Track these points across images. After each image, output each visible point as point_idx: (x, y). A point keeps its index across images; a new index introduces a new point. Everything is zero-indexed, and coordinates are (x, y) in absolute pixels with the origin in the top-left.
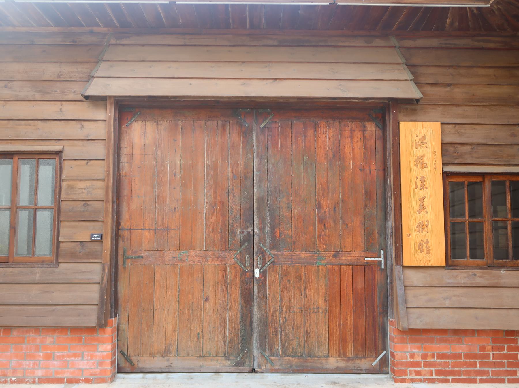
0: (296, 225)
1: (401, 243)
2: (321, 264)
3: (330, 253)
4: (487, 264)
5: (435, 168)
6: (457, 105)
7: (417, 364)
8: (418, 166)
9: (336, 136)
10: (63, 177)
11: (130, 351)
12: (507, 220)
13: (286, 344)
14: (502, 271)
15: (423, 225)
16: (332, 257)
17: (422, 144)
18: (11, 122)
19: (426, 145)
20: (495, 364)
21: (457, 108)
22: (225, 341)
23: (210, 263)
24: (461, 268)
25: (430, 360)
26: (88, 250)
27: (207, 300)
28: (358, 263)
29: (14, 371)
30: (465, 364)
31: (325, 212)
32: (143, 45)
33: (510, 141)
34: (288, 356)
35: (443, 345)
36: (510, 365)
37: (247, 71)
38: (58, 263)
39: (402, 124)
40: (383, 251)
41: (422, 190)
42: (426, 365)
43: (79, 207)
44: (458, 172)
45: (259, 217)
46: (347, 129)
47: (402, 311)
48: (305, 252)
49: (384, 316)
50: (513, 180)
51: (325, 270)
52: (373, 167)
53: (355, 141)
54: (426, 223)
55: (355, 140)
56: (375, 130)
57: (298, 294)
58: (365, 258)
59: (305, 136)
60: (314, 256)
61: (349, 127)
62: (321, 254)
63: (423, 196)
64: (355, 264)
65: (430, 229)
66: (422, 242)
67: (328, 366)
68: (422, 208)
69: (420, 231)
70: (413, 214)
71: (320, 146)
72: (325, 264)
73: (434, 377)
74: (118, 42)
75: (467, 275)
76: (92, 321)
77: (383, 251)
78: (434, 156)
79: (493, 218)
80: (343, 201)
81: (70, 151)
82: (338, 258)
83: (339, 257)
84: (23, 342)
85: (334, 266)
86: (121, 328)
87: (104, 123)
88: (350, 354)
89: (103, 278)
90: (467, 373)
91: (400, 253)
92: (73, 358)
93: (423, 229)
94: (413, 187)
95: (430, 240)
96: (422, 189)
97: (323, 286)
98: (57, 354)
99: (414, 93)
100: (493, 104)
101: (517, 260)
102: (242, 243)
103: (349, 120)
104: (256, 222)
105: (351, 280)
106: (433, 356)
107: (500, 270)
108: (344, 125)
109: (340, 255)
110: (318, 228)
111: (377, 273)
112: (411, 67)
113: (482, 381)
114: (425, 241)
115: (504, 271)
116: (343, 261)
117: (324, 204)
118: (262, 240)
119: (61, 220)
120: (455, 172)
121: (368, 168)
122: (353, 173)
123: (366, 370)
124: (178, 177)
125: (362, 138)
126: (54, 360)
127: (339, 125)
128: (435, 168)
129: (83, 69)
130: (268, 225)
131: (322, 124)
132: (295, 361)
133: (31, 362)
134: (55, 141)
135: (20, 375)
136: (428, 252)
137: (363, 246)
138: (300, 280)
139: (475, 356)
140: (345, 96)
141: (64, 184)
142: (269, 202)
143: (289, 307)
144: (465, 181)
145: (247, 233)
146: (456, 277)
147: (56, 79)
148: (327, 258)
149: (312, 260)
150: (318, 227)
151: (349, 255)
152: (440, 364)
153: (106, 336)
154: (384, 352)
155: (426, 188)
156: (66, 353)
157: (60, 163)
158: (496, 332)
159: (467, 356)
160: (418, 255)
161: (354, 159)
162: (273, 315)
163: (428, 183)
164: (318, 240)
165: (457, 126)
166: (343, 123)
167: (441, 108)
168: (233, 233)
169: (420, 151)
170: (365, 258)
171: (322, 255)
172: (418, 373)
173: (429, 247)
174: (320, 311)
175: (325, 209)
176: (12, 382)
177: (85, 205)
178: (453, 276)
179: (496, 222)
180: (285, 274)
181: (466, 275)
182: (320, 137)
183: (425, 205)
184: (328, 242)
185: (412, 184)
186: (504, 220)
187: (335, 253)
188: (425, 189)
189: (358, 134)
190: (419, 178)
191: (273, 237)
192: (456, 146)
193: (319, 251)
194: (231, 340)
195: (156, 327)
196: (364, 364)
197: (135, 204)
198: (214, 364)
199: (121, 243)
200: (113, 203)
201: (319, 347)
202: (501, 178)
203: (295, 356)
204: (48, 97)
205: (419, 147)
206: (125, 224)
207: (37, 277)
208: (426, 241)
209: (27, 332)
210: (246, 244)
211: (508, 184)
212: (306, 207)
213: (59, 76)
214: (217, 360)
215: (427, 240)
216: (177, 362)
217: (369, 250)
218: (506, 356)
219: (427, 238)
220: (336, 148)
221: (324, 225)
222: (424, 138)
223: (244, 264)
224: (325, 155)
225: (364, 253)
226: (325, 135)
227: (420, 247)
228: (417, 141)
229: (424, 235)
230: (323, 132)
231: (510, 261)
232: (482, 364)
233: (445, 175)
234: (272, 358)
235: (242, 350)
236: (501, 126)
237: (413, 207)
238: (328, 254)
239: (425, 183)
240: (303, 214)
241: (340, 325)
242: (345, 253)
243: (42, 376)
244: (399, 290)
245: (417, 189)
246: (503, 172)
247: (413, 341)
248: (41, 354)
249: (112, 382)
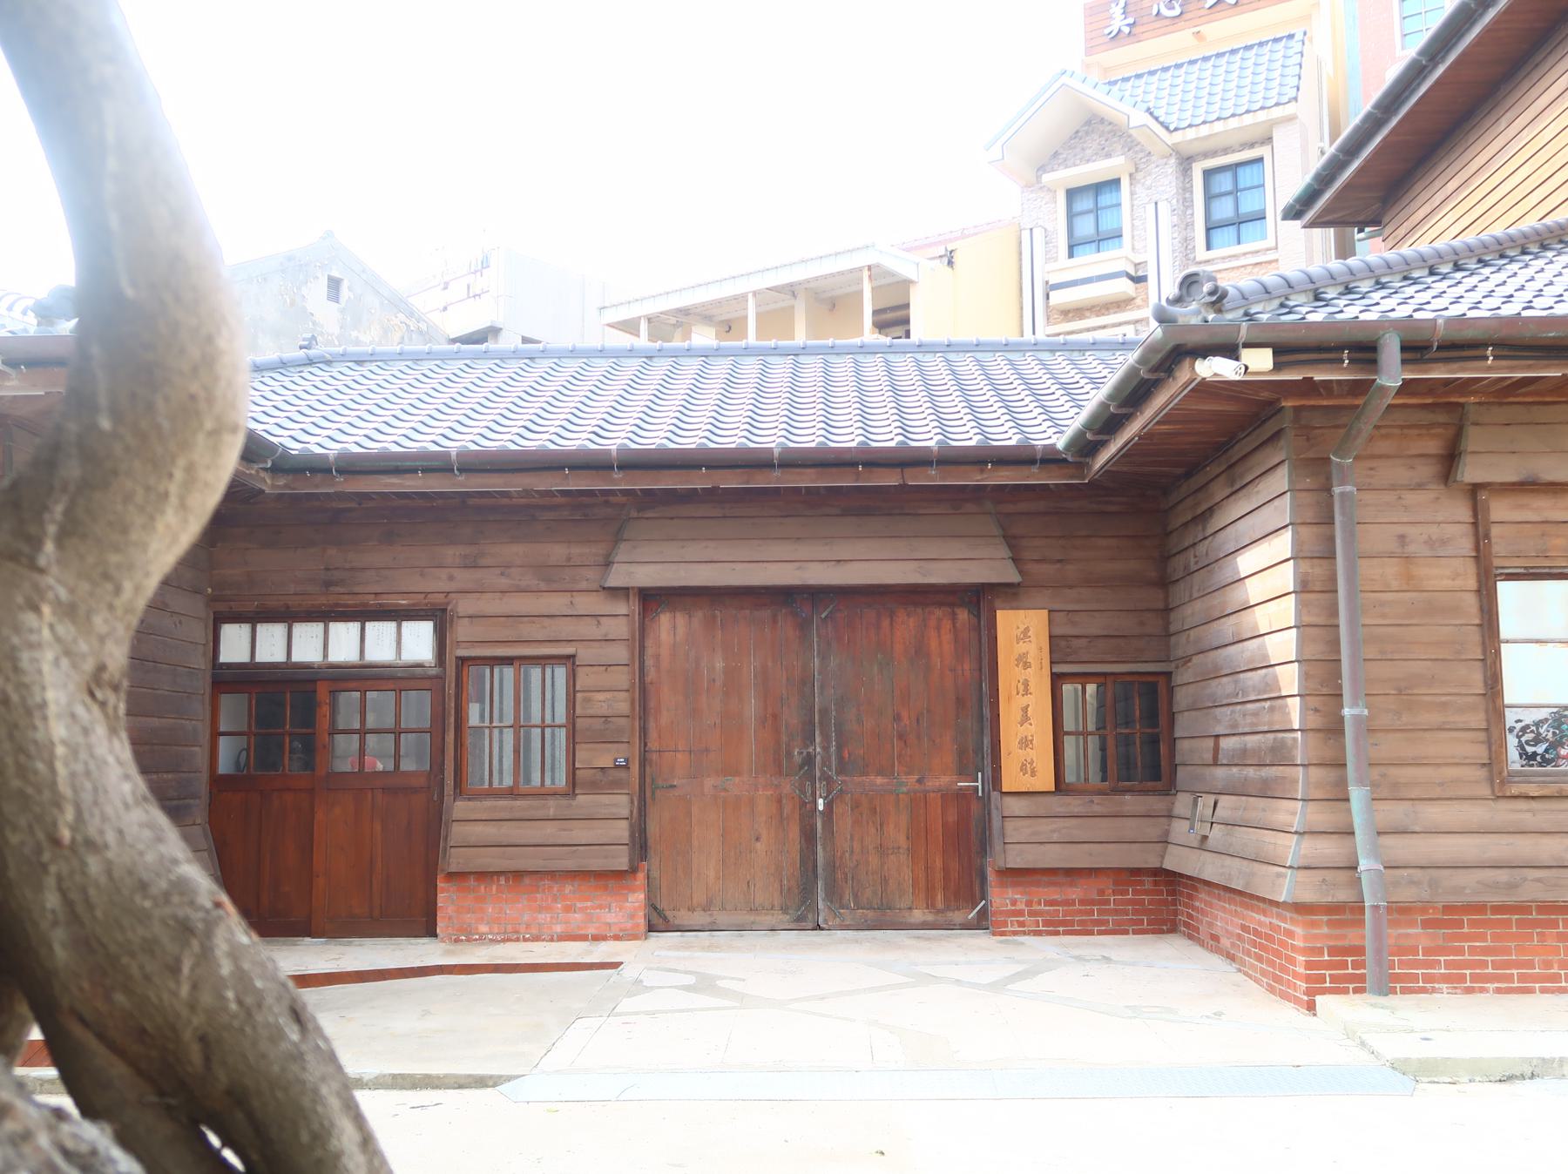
5: (1042, 668)
6: (1070, 587)
7: (1020, 913)
10: (577, 689)
11: (663, 904)
13: (859, 894)
18: (510, 618)
20: (1116, 912)
22: (781, 893)
23: (760, 793)
25: (1035, 907)
26: (611, 778)
27: (758, 839)
29: (528, 926)
30: (1081, 912)
32: (672, 518)
34: (862, 909)
35: (1052, 889)
36: (1136, 912)
37: (804, 551)
38: (575, 795)
39: (999, 613)
40: (980, 774)
42: (1032, 913)
43: (598, 724)
45: (822, 733)
47: (998, 847)
49: (983, 857)
52: (967, 666)
54: (1030, 738)
57: (873, 830)
67: (912, 920)
68: (1025, 719)
73: (1041, 928)
74: (640, 515)
76: (622, 863)
77: (980, 774)
81: (585, 654)
84: (537, 892)
85: (918, 795)
86: (651, 876)
87: (625, 618)
88: (940, 905)
89: (632, 812)
90: (1081, 923)
92: (598, 911)
93: (1027, 746)
95: (1034, 759)
97: (904, 819)
98: (579, 905)
99: (1012, 576)
102: (801, 767)
104: (818, 740)
105: (939, 811)
106: (1040, 904)
112: (1012, 541)
113: (1101, 933)
114: (1029, 760)
117: (904, 714)
118: (826, 762)
119: (576, 741)
123: (960, 924)
124: (719, 683)
126: (575, 912)
129: (598, 550)
130: (834, 743)
132: (870, 914)
133: (548, 915)
134: (565, 643)
135: (535, 931)
136: (1033, 774)
138: (876, 812)
139: (1092, 902)
140: (926, 582)
141: (579, 695)
142: (834, 713)
143: (862, 847)
145: (37, 315)
147: (564, 564)
152: (1048, 912)
153: (638, 883)
154: (984, 902)
155: (1030, 693)
156: (589, 904)
157: (573, 670)
158: (1118, 871)
159: (1082, 902)
162: (841, 858)
163: (1032, 689)
168: (789, 754)
169: (1022, 647)
172: (1021, 924)
174: (901, 851)
175: (906, 721)
176: (525, 940)
177: (606, 722)
180: (856, 805)
189: (947, 624)
190: (1021, 681)
191: (840, 759)
192: (1069, 639)
194: (789, 889)
195: (695, 875)
196: (958, 917)
197: (665, 719)
198: (769, 919)
199: (648, 769)
200: (640, 718)
201: (900, 897)
202: (1128, 678)
203: (871, 908)
204: (555, 586)
206: (653, 744)
207: (551, 813)
209: (542, 879)
210: (806, 768)
213: (569, 559)
214: (773, 915)
216: (722, 918)
217: (963, 772)
218: (1131, 902)
222: (1027, 630)
223: (804, 793)
227: (1023, 768)
232: (1100, 912)
234: (842, 911)
235: (803, 903)
241: (927, 868)
243: (562, 932)
244: (996, 822)
247: (1014, 885)
248: (559, 906)
249: (646, 939)
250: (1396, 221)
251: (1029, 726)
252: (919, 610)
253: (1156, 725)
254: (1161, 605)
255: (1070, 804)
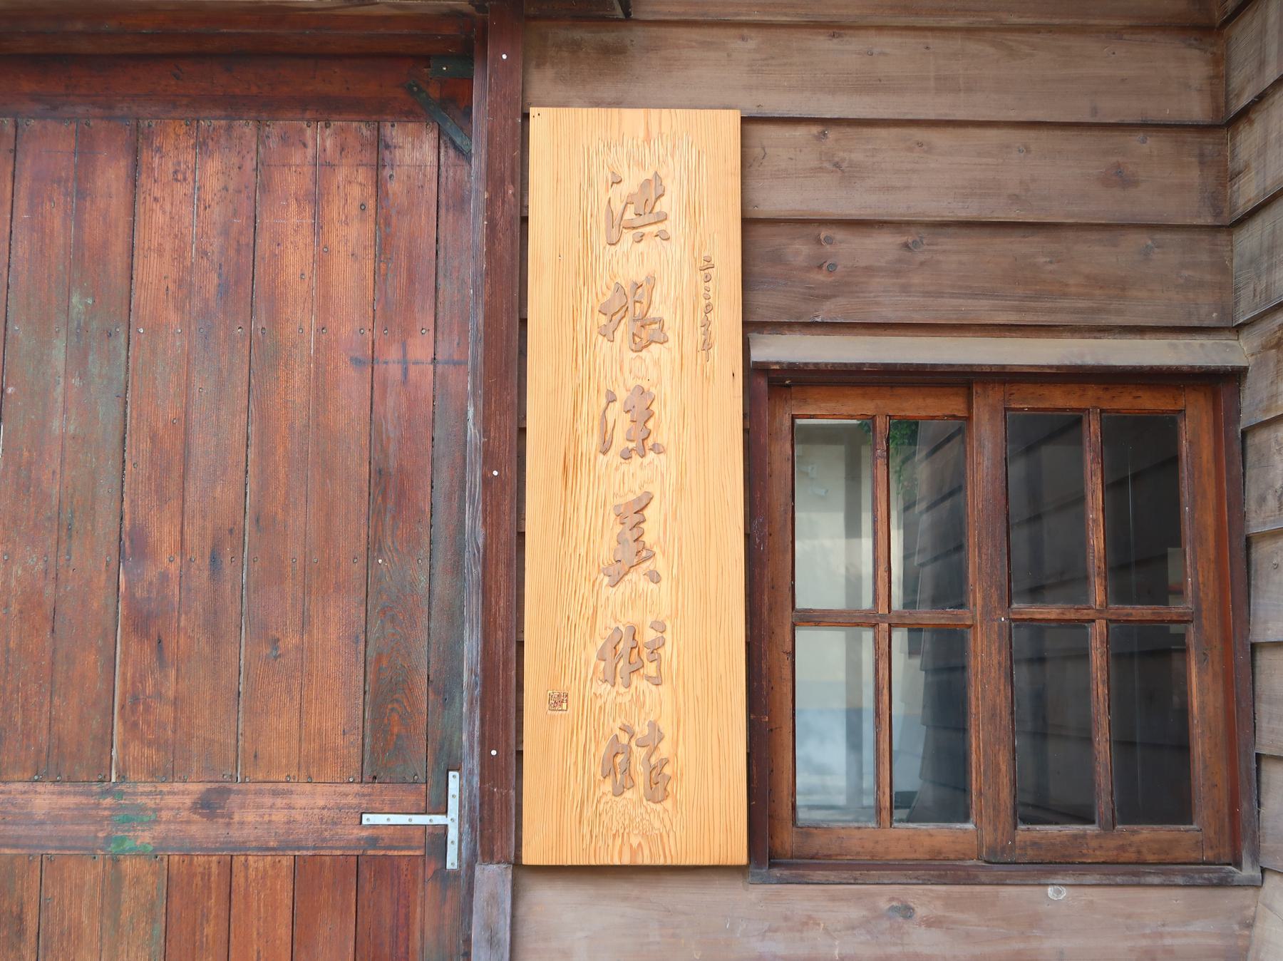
0: (12, 645)
1: (513, 742)
2: (131, 849)
3: (183, 793)
4: (980, 846)
5: (707, 346)
6: (835, 28)
8: (618, 334)
9: (240, 192)
12: (1086, 614)
14: (1050, 890)
15: (631, 644)
16: (190, 809)
17: (639, 221)
19: (661, 226)
21: (835, 40)
24: (832, 875)
28: (324, 840)
31: (164, 577)
33: (1105, 205)
41: (636, 459)
44: (826, 364)
46: (296, 157)
48: (50, 787)
50: (1118, 411)
51: (150, 879)
53: (335, 216)
54: (649, 635)
55: (334, 211)
56: (436, 163)
58: (365, 816)
59: (82, 194)
60: (97, 806)
61: (305, 145)
62: (134, 794)
63: (639, 493)
64: (307, 849)
65: (670, 666)
66: (624, 739)
69: (619, 680)
70: (585, 589)
71: (155, 244)
72: (150, 848)
75: (865, 913)
78: (702, 285)
79: (1015, 605)
80: (258, 521)
82: (223, 816)
83: (225, 811)
91: (507, 795)
94: (590, 443)
95: (666, 727)
96: (633, 454)
100: (1014, 20)
101: (1135, 827)
103: (308, 115)
105: (284, 932)
107: (1043, 881)
108: (284, 139)
109: (234, 800)
110: (124, 663)
111: (420, 893)
114: (642, 730)
115: (1064, 890)
116: (245, 832)
117: (163, 534)
120: (812, 367)
121: (394, 353)
122: (317, 378)
125: (371, 204)
127: (255, 139)
128: (707, 346)
131: (170, 130)
136: (658, 786)
137: (355, 751)
138: (21, 933)
144: (873, 417)
146: (806, 924)
148: (165, 815)
149: (83, 829)
150: (126, 653)
151: (279, 802)
155: (658, 449)
160: (601, 806)
161: (324, 304)
163: (664, 429)
164: (125, 723)
165: (832, 134)
166: (275, 129)
167: (751, 44)
170: (365, 816)
171: (141, 800)
173: (665, 762)
175: (167, 561)
178: (786, 919)
179: (1038, 628)
181: (855, 913)
182: (156, 199)
183: (648, 539)
184: (175, 732)
185: (581, 427)
186: (1071, 615)
187: (208, 790)
188: (651, 455)
190: (622, 395)
192: (824, 233)
193: (122, 778)
202: (1059, 399)
205: (628, 236)
208: (646, 732)
211: (1093, 429)
212: (69, 553)
215: (653, 725)
219: (652, 718)
220: (238, 251)
221: (155, 644)
222: (653, 189)
224: (180, 286)
225: (356, 787)
226: (181, 189)
228: (618, 206)
229: (638, 697)
230: (175, 172)
231: (1097, 836)
233: (763, 383)
236: (1058, 133)
237: (583, 553)
238: (169, 793)
239: (650, 425)
240: (49, 591)
242: (259, 793)
245: (611, 453)
246: (1058, 367)
250: (972, 655)
251: (645, 585)
252: (246, 129)
253: (1160, 592)
254: (1196, 109)
255: (808, 922)
